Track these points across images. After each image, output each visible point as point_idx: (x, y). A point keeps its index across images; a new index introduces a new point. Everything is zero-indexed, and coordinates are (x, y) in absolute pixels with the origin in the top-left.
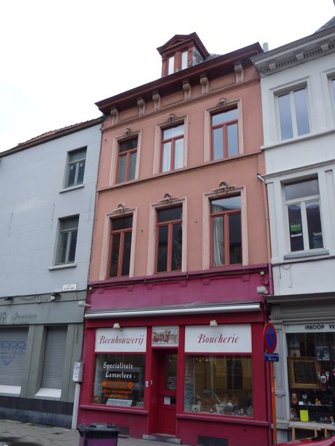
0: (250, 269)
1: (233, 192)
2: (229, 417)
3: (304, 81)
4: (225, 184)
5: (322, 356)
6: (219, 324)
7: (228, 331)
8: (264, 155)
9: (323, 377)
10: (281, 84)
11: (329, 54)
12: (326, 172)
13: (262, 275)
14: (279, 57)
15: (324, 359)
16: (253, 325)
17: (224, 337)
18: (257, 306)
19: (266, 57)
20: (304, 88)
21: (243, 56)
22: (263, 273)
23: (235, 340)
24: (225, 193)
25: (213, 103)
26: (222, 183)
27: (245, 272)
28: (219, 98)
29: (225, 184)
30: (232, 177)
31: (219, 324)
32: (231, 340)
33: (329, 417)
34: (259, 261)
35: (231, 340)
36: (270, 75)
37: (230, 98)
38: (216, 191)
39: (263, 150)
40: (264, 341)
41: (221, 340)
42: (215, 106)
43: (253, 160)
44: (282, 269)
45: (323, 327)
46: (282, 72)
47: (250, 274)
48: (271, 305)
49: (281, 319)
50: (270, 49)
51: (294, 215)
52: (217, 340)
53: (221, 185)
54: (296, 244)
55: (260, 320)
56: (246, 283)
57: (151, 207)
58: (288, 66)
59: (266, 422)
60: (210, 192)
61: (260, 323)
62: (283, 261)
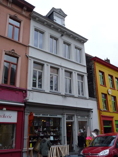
0: (20, 89)
1: (16, 55)
2: (2, 151)
3: (44, 32)
4: (14, 51)
5: (36, 124)
6: (7, 110)
7: (8, 113)
8: (29, 48)
9: (37, 131)
10: (38, 27)
11: (36, 21)
12: (47, 65)
13: (24, 93)
14: (41, 18)
15: (36, 125)
16: (18, 112)
17: (5, 115)
18: (24, 105)
19: (52, 22)
20: (42, 34)
21: (29, 7)
22: (24, 92)
23: (10, 117)
24: (13, 54)
25: (13, 14)
26: (13, 50)
27: (18, 90)
28: (15, 14)
29: (14, 51)
30: (19, 51)
31: (7, 110)
32: (8, 117)
33: (5, 147)
34: (23, 87)
35: (8, 117)
36: (34, 21)
37: (19, 17)
38: (10, 51)
39: (29, 46)
40: (20, 118)
41: (4, 116)
42: (13, 15)
43: (25, 47)
44: (30, 92)
45: (40, 115)
46: (39, 23)
47: (19, 91)
48: (28, 105)
49: (29, 110)
50: (56, 22)
51: (35, 73)
52: (2, 117)
53: (12, 50)
54: (34, 85)
55: (22, 110)
56: (17, 94)
57: (3, 51)
58: (40, 23)
59: (21, 150)
60: (7, 51)
61: (22, 111)
62: (31, 90)
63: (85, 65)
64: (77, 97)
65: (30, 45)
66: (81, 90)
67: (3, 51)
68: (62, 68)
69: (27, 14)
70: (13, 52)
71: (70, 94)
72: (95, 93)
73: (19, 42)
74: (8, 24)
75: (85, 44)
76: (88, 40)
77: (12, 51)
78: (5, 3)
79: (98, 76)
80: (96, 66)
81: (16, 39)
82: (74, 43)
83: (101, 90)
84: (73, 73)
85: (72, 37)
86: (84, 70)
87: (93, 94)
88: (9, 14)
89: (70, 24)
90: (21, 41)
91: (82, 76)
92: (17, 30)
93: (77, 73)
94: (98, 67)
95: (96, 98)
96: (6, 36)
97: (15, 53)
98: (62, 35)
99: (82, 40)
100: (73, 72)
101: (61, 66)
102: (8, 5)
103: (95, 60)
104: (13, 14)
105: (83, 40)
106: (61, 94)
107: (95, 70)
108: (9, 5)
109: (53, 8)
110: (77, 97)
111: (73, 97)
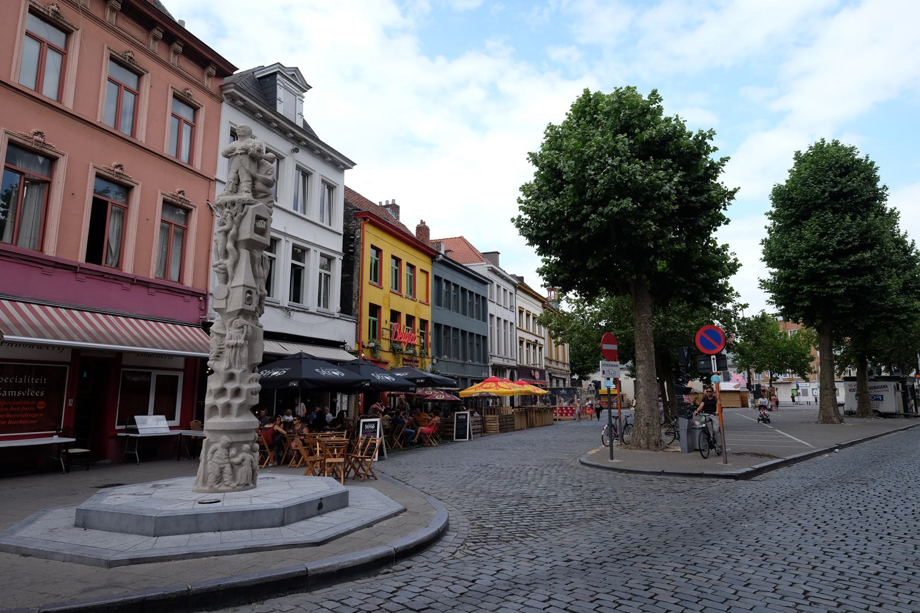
25: (121, 47)
26: (119, 166)
29: (42, 137)
34: (200, 288)
43: (206, 182)
57: (159, 194)
60: (101, 167)
63: (341, 230)
64: (314, 314)
65: (219, 176)
66: (323, 298)
67: (159, 194)
68: (287, 239)
69: (211, 84)
70: (119, 174)
71: (325, 310)
72: (354, 303)
73: (133, 141)
74: (104, 78)
75: (346, 171)
76: (354, 164)
77: (37, 137)
78: (97, 11)
79: (368, 255)
80: (366, 233)
81: (49, 91)
82: (320, 170)
83: (370, 294)
84: (283, 242)
85: (277, 128)
86: (336, 244)
87: (348, 307)
88: (108, 48)
89: (318, 113)
90: (68, 104)
91: (330, 259)
92: (53, 59)
93: (319, 251)
94: (371, 236)
95: (357, 316)
96: (12, 79)
97: (47, 142)
98: (296, 150)
99: (340, 163)
100: (312, 248)
101: (286, 235)
102: (104, 17)
103: (365, 219)
104: (181, 85)
105: (343, 164)
106: (281, 305)
107: (363, 244)
108: (109, 17)
109: (498, 253)
110: (314, 314)
111: (305, 311)
